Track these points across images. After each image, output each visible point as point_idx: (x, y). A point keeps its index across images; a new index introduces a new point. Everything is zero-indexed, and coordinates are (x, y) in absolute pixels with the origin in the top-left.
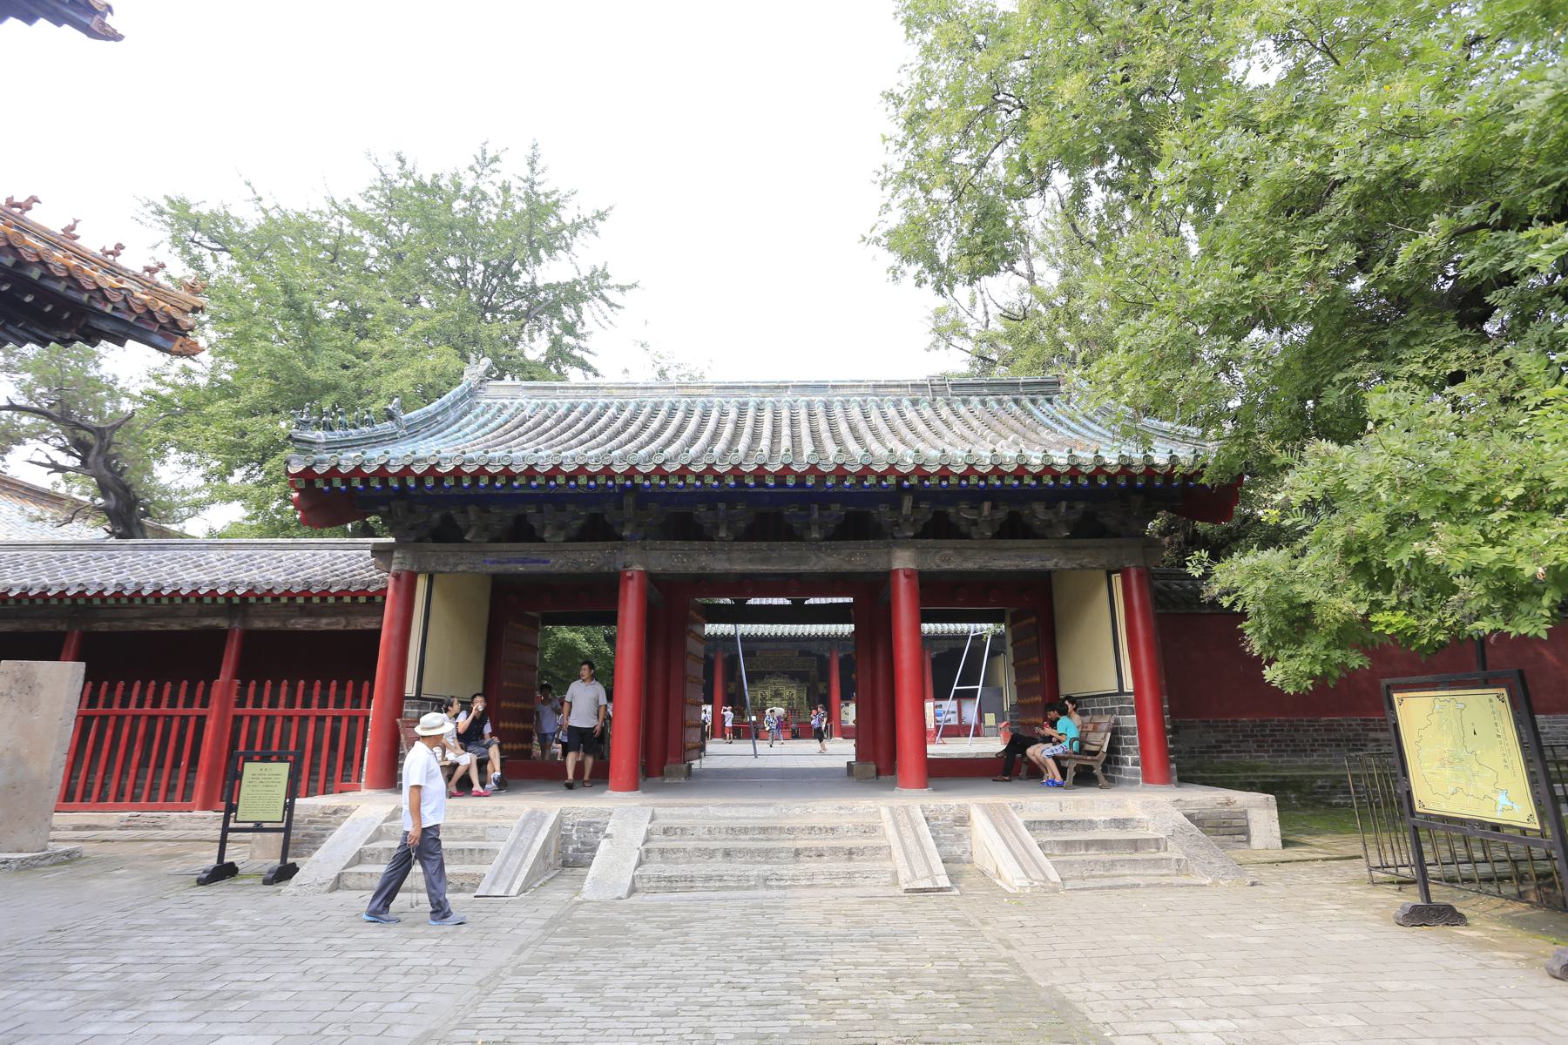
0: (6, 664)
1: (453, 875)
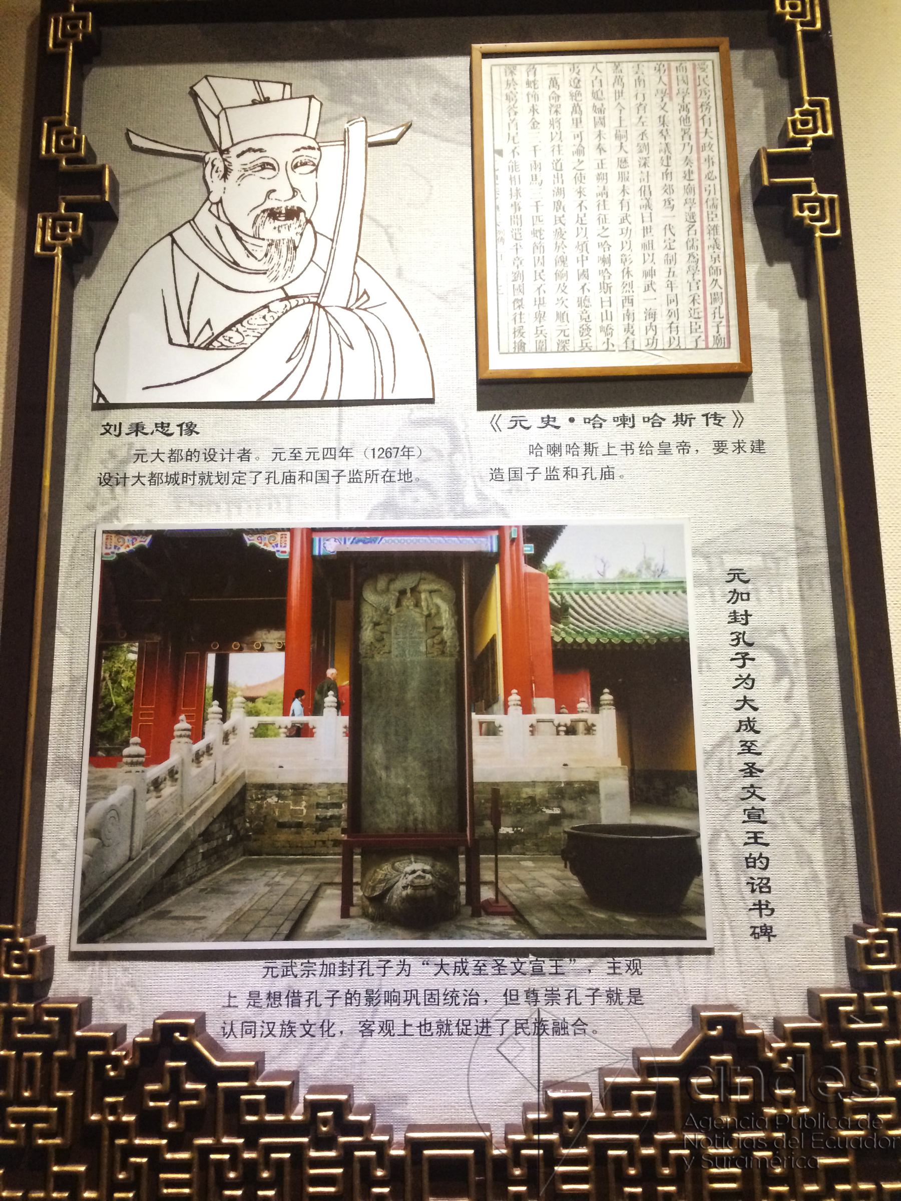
0: (38, 3)
1: (339, 854)
